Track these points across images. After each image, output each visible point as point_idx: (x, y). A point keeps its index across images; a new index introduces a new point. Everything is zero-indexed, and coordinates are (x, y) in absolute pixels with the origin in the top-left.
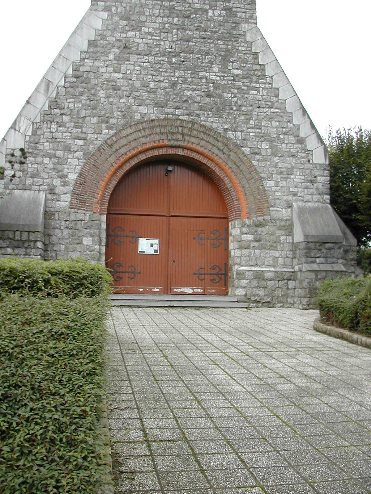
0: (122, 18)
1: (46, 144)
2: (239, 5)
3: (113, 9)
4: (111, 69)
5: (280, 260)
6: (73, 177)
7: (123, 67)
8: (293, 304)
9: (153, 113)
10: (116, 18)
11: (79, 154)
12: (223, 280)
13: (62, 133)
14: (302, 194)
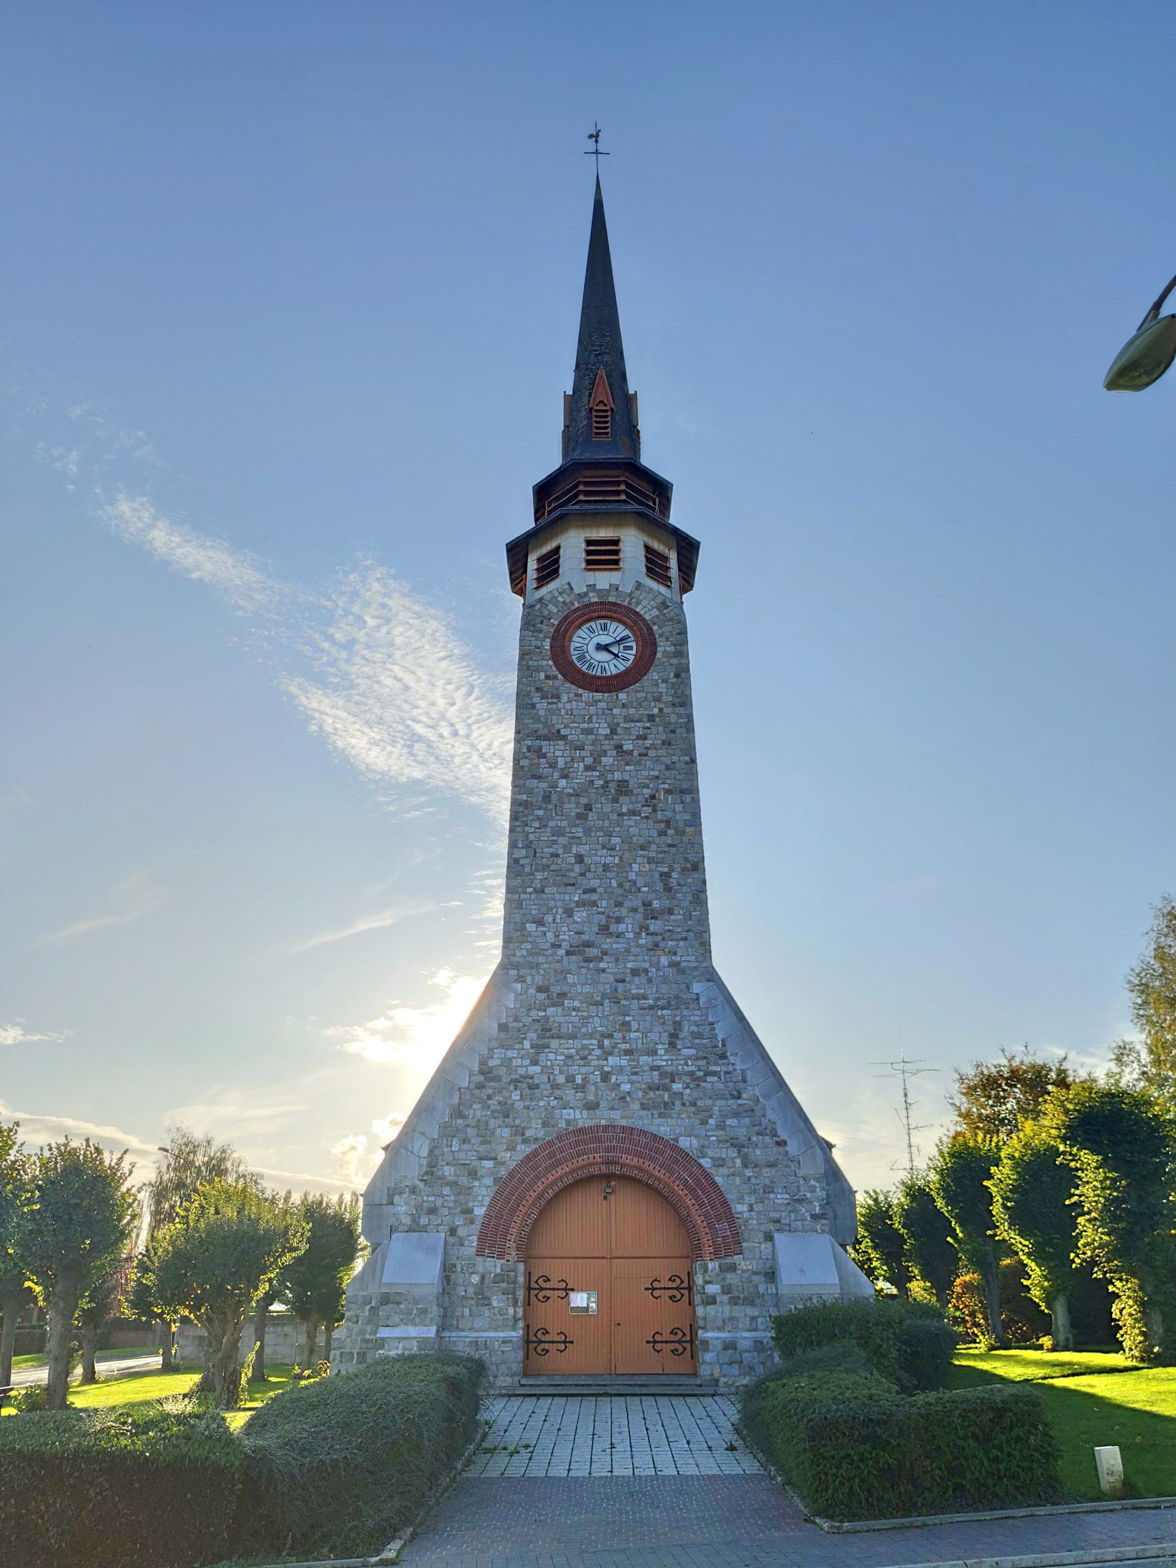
0: (540, 989)
1: (446, 1168)
2: (689, 958)
3: (529, 979)
4: (527, 1062)
5: (760, 1320)
6: (480, 1211)
7: (542, 1057)
8: (504, 1342)
9: (583, 1119)
10: (532, 991)
11: (489, 1181)
12: (534, 1279)
13: (467, 1151)
14: (787, 1221)
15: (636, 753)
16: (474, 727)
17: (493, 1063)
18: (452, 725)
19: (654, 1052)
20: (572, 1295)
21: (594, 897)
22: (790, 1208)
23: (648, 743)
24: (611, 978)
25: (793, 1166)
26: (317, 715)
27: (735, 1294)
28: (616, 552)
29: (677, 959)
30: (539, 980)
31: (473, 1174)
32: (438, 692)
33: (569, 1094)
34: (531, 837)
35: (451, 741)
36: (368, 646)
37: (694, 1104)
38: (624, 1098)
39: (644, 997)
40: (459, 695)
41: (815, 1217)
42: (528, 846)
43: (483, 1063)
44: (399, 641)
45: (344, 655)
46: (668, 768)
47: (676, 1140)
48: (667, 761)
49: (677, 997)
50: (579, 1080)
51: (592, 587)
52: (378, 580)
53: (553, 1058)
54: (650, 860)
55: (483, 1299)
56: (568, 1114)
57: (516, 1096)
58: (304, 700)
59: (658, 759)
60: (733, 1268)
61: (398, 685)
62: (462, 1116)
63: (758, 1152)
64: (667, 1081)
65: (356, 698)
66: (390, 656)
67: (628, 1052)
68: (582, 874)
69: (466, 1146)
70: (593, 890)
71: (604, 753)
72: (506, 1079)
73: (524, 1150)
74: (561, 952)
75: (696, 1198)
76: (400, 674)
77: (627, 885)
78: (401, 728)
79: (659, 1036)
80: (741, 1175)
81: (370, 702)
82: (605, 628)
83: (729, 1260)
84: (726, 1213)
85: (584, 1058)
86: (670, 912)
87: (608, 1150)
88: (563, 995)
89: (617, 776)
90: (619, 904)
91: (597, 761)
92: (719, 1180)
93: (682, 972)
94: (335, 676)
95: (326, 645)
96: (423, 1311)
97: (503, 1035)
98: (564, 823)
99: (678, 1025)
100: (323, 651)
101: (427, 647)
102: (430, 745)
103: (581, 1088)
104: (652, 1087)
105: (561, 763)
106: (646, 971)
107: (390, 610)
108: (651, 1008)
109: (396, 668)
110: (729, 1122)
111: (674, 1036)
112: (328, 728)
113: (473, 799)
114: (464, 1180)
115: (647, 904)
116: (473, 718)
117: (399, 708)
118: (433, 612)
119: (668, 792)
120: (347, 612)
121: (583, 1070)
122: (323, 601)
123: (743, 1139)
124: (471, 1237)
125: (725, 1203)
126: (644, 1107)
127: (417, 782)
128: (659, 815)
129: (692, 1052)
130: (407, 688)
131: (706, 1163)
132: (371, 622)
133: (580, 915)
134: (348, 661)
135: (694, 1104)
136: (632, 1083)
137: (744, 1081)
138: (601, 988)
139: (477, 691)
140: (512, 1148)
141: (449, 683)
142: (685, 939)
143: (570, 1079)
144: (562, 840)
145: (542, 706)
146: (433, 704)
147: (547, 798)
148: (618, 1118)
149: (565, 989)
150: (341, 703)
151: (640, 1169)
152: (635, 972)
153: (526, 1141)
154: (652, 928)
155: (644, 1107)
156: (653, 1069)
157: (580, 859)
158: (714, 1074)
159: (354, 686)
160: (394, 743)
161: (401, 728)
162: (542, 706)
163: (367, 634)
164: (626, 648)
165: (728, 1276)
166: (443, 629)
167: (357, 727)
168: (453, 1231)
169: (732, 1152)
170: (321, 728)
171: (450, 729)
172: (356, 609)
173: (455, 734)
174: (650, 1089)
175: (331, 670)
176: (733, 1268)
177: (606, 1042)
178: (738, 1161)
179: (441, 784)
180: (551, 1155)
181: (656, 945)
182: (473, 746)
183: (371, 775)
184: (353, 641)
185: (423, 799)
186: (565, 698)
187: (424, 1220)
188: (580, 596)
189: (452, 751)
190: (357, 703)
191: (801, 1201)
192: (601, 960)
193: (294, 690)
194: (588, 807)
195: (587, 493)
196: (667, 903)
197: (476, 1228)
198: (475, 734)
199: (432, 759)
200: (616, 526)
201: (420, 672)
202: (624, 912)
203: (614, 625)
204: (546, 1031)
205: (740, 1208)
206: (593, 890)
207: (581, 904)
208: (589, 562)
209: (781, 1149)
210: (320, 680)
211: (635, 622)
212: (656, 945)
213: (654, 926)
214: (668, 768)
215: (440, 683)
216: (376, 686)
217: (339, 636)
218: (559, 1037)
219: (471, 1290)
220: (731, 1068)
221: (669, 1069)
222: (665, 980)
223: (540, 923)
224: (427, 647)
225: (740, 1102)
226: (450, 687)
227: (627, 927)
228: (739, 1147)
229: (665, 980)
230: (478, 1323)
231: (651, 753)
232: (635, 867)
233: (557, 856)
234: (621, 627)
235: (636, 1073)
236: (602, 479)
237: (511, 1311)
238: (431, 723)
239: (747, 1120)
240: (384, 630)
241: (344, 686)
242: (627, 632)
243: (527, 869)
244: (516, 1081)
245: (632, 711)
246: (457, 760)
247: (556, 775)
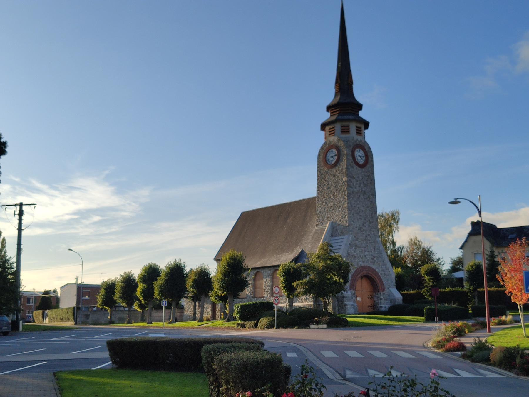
9: (363, 264)
28: (349, 129)
42: (351, 204)
103: (362, 258)
111: (374, 249)
112: (484, 341)
133: (360, 221)
145: (351, 169)
157: (359, 208)
162: (351, 169)
169: (383, 273)
205: (384, 283)
208: (342, 132)
213: (371, 225)
228: (384, 271)
236: (345, 110)
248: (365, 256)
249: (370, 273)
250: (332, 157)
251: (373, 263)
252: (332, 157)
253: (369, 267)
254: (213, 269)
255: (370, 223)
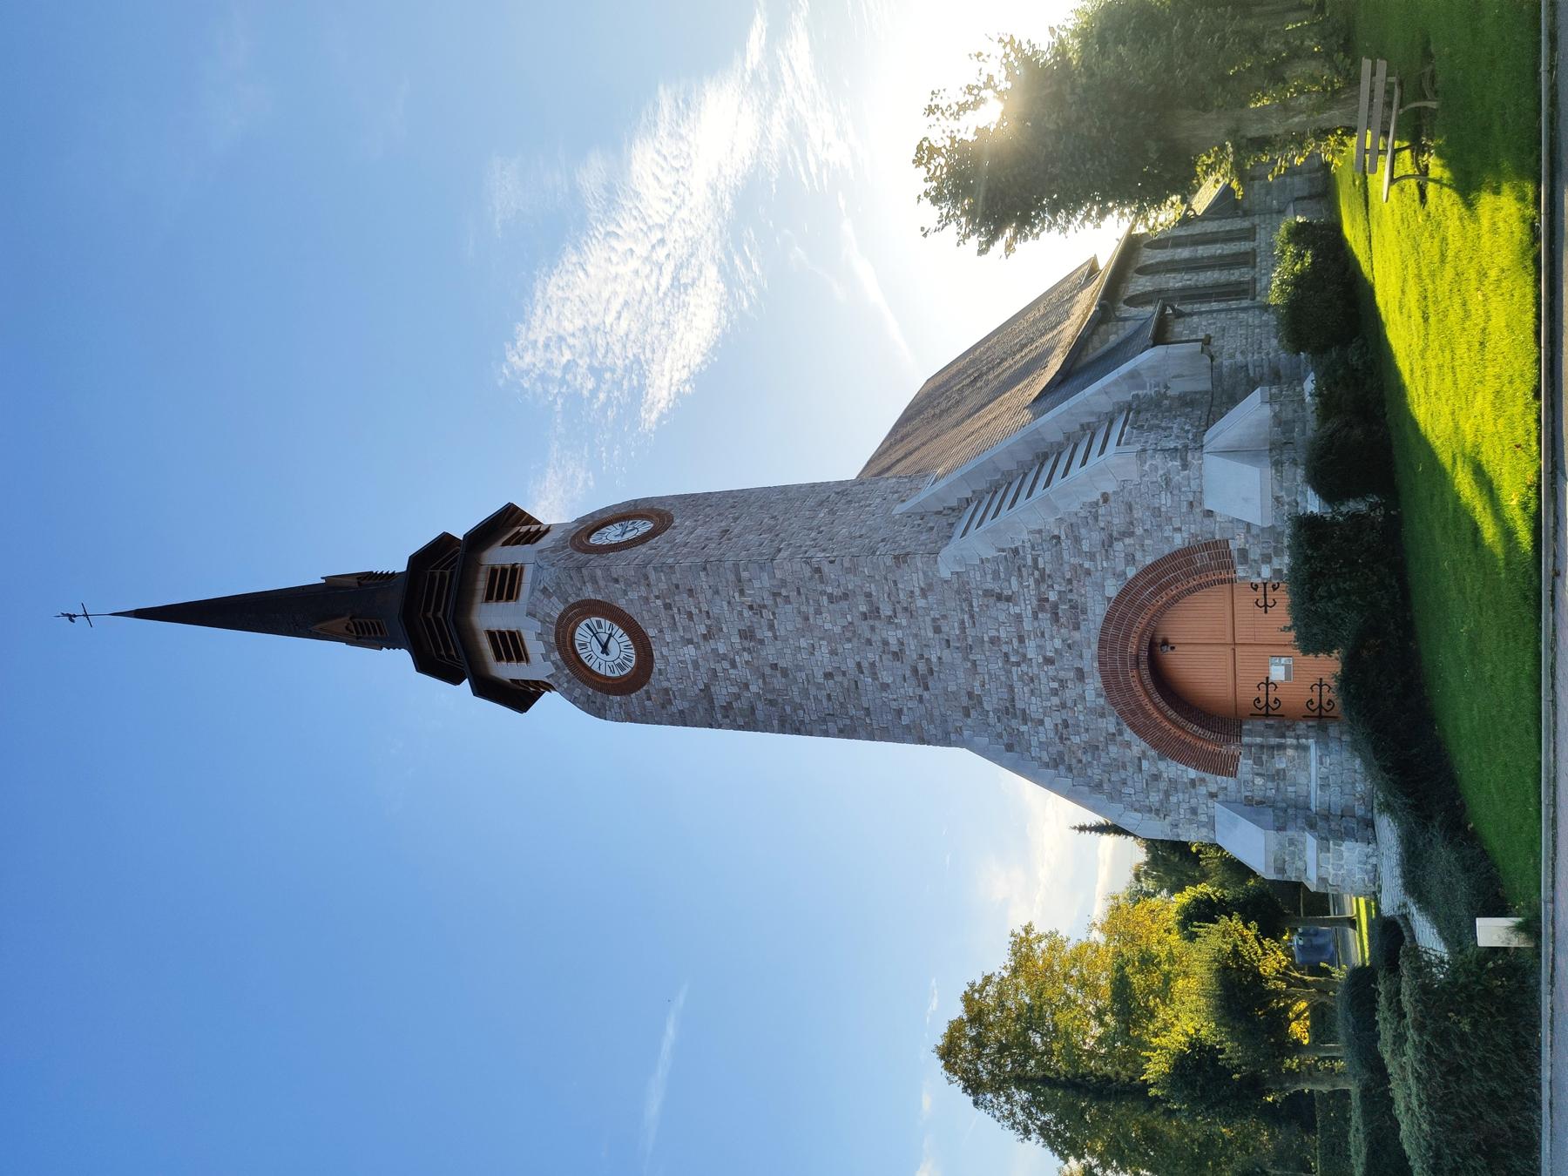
6: (1192, 773)
9: (1094, 684)
10: (969, 721)
11: (1162, 765)
15: (708, 622)
16: (650, 222)
17: (1046, 758)
18: (653, 247)
19: (1019, 618)
20: (1272, 679)
21: (865, 664)
22: (1176, 492)
23: (695, 611)
24: (946, 651)
25: (1129, 487)
26: (674, 389)
27: (1270, 551)
29: (917, 592)
30: (959, 715)
31: (1156, 777)
32: (621, 269)
33: (1070, 693)
34: (814, 717)
35: (670, 245)
36: (593, 354)
37: (1070, 581)
38: (1069, 646)
39: (963, 622)
40: (620, 246)
41: (1185, 466)
43: (1047, 765)
44: (579, 323)
45: (608, 375)
46: (717, 592)
47: (1109, 599)
48: (709, 593)
49: (958, 592)
50: (1055, 685)
51: (545, 658)
52: (521, 358)
53: (1035, 707)
54: (818, 612)
55: (1279, 776)
56: (1090, 695)
57: (1076, 739)
58: (662, 404)
59: (709, 602)
60: (1244, 553)
61: (625, 314)
62: (1100, 785)
63: (1116, 521)
64: (1047, 606)
65: (649, 354)
66: (597, 329)
67: (1021, 640)
68: (844, 674)
69: (1130, 783)
70: (859, 665)
71: (715, 651)
72: (1061, 747)
73: (1128, 734)
74: (926, 695)
75: (1168, 585)
76: (613, 314)
77: (849, 635)
78: (668, 302)
79: (1001, 611)
80: (1142, 538)
81: (648, 339)
82: (584, 645)
83: (1235, 554)
84: (1186, 554)
85: (1032, 680)
86: (869, 595)
87: (1124, 663)
88: (970, 695)
89: (736, 639)
90: (869, 642)
91: (724, 657)
92: (1149, 560)
93: (930, 585)
94: (630, 379)
95: (602, 396)
96: (1292, 842)
97: (1017, 748)
98: (795, 689)
99: (987, 593)
100: (609, 397)
101: (577, 292)
102: (679, 267)
103: (1063, 683)
104: (1056, 617)
105: (735, 690)
106: (934, 620)
107: (549, 339)
108: (972, 617)
109: (609, 319)
110: (1085, 548)
111: (999, 597)
112: (685, 374)
113: (728, 206)
114: (1163, 785)
115: (865, 616)
116: (642, 225)
117: (649, 308)
118: (539, 294)
119: (742, 592)
120: (563, 382)
121: (1044, 681)
122: (558, 407)
123: (1103, 535)
124: (1215, 782)
125: (1173, 556)
126: (1077, 627)
127: (721, 270)
128: (769, 602)
129: (1014, 581)
130: (626, 303)
131: (1131, 572)
132: (567, 356)
134: (613, 371)
135: (1070, 581)
136: (1052, 637)
137: (1040, 532)
138: (958, 661)
139: (612, 228)
140: (1128, 745)
141: (610, 260)
142: (895, 582)
143: (1055, 692)
144: (813, 691)
146: (637, 272)
147: (772, 703)
148: (1090, 652)
149: (963, 693)
150: (655, 368)
151: (1141, 636)
152: (937, 630)
153: (1121, 733)
154: (890, 613)
155: (1077, 627)
156: (1035, 617)
158: (1035, 561)
159: (637, 359)
160: (685, 305)
161: (668, 302)
162: (679, 704)
163: (581, 357)
164: (600, 625)
165: (1252, 557)
166: (554, 280)
167: (677, 346)
168: (1213, 795)
169: (1118, 546)
170: (687, 380)
171: (658, 249)
172: (558, 374)
173: (662, 241)
174: (1057, 621)
175: (625, 383)
176: (1244, 553)
177: (1013, 659)
178: (1128, 541)
179: (718, 245)
180: (1133, 713)
181: (906, 609)
182: (670, 220)
183: (724, 322)
184: (591, 368)
185: (737, 261)
186: (665, 684)
187: (1204, 818)
188: (557, 668)
189: (682, 240)
190: (653, 352)
191: (1168, 482)
192: (928, 660)
193: (654, 416)
194: (774, 666)
195: (447, 649)
196: (861, 599)
197: (1208, 777)
198: (658, 220)
199: (693, 261)
200: (476, 643)
201: (605, 295)
202: (876, 638)
203: (577, 636)
204: (1008, 709)
205: (1179, 541)
206: (859, 665)
207: (874, 676)
208: (509, 598)
209: (1112, 498)
210: (638, 393)
211: (570, 620)
212: (906, 609)
213: (886, 611)
214: (717, 592)
215: (613, 270)
216: (632, 337)
217: (590, 384)
218: (1013, 700)
219: (1270, 785)
220: (1028, 545)
221: (1035, 603)
222: (942, 602)
223: (900, 712)
224: (577, 292)
225: (1063, 537)
226: (615, 259)
227: (893, 636)
229: (942, 602)
230: (1302, 780)
231: (705, 608)
232: (828, 626)
233: (829, 696)
234: (578, 630)
235: (1043, 634)
237: (1290, 752)
238: (656, 271)
239: (1083, 531)
240: (571, 341)
241: (638, 367)
242: (583, 624)
243: (848, 722)
244: (1061, 738)
245: (665, 624)
246: (690, 233)
247: (747, 694)
248: (1049, 661)
249: (1132, 648)
250: (605, 649)
251: (1077, 610)
252: (605, 649)
253: (1102, 644)
254: (1070, 947)
255: (875, 612)
